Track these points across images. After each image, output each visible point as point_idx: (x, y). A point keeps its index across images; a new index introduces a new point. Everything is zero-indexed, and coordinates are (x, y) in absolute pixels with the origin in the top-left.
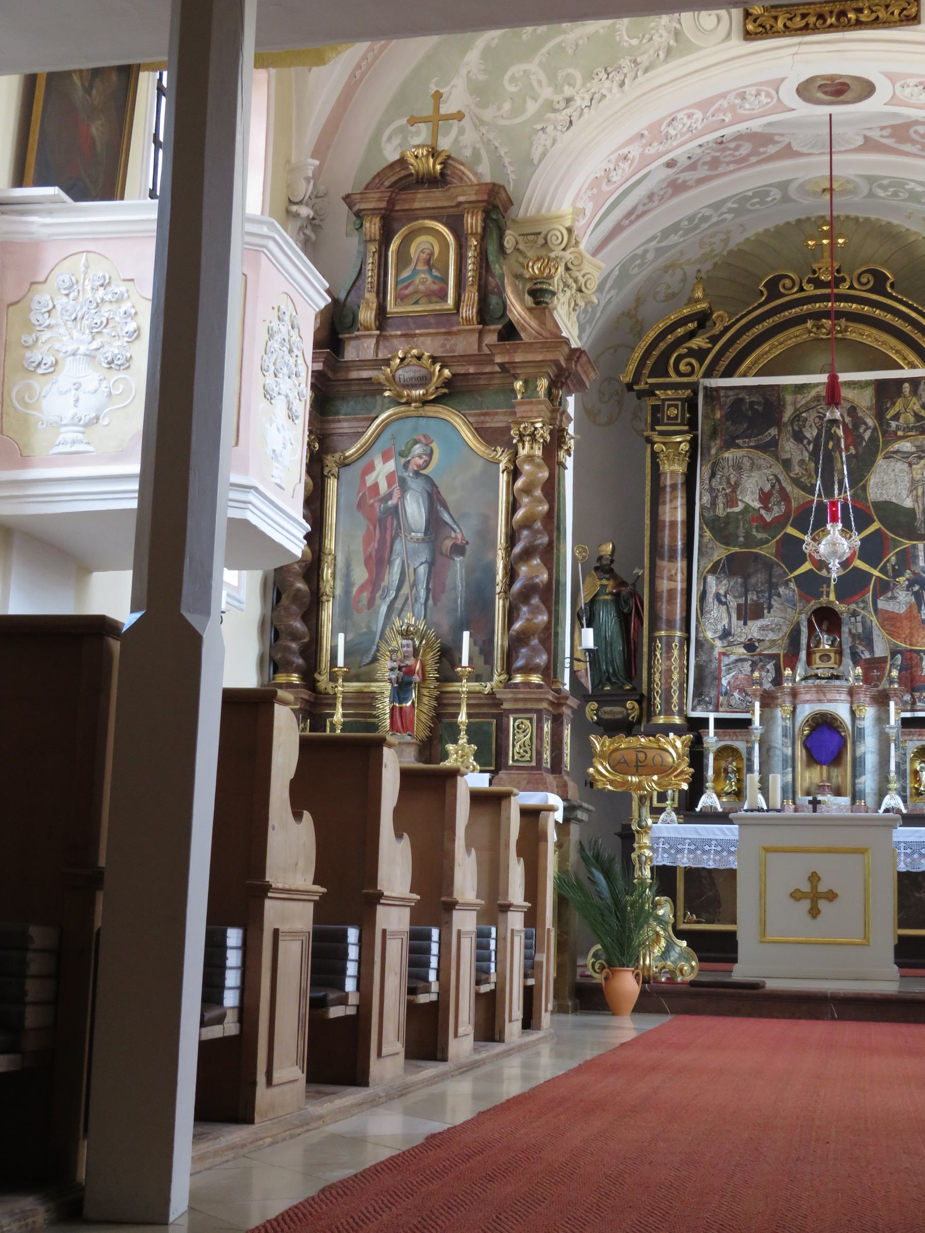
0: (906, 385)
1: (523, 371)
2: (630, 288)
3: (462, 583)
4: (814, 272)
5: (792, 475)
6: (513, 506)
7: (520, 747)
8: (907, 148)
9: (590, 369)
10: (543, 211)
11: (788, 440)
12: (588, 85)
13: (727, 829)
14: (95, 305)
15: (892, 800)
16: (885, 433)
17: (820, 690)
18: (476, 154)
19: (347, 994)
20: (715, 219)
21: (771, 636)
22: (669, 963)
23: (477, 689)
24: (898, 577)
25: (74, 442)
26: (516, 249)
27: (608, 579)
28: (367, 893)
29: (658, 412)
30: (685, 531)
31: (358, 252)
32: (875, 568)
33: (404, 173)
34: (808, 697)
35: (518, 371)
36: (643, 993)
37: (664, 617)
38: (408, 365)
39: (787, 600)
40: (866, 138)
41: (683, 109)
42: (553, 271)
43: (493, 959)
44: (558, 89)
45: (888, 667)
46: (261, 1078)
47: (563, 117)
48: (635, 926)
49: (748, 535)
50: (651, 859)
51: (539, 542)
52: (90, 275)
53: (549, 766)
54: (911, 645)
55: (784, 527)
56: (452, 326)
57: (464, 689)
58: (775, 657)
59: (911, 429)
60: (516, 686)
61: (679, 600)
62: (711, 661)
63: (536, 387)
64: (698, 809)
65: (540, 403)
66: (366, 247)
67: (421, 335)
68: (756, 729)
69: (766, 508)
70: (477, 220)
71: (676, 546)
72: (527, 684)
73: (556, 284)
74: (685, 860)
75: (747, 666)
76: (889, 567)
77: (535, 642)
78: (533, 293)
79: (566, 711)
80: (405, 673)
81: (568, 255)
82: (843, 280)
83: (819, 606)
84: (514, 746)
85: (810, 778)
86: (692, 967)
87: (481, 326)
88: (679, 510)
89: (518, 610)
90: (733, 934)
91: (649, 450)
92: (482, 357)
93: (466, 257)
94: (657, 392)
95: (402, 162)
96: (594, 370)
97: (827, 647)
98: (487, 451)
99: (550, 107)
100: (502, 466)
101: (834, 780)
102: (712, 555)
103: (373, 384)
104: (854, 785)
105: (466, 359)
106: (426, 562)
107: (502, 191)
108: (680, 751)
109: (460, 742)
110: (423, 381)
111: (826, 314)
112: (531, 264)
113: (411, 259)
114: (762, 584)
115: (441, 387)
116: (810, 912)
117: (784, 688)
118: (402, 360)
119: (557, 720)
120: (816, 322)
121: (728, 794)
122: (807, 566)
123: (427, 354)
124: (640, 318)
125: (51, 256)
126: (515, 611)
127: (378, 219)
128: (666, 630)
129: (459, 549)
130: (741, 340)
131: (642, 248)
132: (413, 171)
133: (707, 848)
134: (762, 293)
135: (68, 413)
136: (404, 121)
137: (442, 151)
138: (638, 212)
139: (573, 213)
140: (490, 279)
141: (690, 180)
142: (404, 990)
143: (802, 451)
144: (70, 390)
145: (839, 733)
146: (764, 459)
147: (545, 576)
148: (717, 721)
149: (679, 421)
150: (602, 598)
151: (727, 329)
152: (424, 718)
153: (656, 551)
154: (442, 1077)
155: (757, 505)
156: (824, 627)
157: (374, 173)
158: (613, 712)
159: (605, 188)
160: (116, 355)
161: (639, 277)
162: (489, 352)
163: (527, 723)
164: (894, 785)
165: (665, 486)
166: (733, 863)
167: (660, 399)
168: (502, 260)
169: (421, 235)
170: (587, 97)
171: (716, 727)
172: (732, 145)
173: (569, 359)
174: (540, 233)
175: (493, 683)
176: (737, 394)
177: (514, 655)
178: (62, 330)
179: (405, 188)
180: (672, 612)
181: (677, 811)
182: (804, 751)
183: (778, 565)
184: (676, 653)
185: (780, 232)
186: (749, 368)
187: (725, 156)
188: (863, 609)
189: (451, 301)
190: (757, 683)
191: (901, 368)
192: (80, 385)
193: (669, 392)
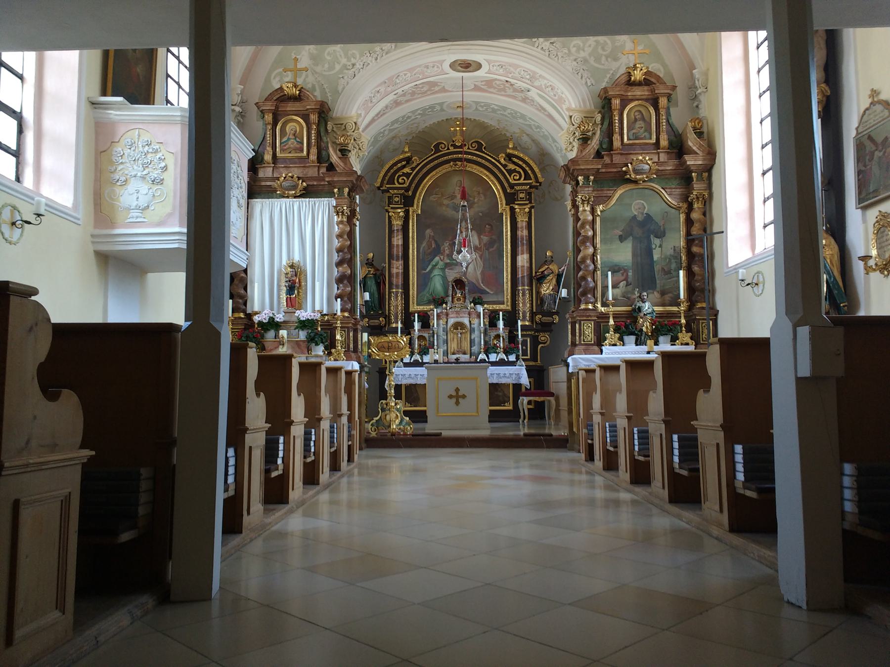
2: (378, 146)
4: (454, 141)
8: (492, 90)
12: (362, 58)
14: (144, 154)
18: (314, 86)
20: (413, 118)
22: (402, 426)
25: (137, 217)
31: (263, 128)
33: (282, 94)
34: (452, 316)
37: (394, 284)
38: (287, 180)
40: (475, 85)
41: (402, 72)
43: (335, 432)
44: (349, 60)
46: (245, 513)
47: (351, 72)
52: (141, 140)
53: (352, 350)
63: (344, 191)
65: (345, 198)
66: (266, 126)
73: (350, 147)
81: (355, 135)
82: (465, 145)
86: (411, 428)
87: (319, 164)
90: (425, 411)
91: (387, 215)
94: (390, 191)
95: (281, 89)
97: (460, 295)
99: (345, 67)
101: (463, 348)
103: (272, 188)
105: (312, 178)
107: (326, 104)
110: (294, 187)
111: (460, 160)
112: (339, 138)
113: (286, 133)
116: (451, 395)
118: (285, 178)
120: (454, 163)
123: (295, 176)
124: (383, 159)
125: (121, 130)
127: (271, 114)
131: (383, 129)
135: (134, 204)
136: (281, 70)
138: (381, 114)
140: (322, 143)
142: (302, 457)
144: (134, 193)
147: (349, 272)
150: (369, 276)
151: (418, 165)
153: (391, 257)
154: (318, 493)
157: (268, 94)
158: (375, 322)
159: (370, 105)
160: (156, 178)
161: (382, 141)
163: (343, 332)
167: (391, 194)
170: (362, 64)
172: (421, 86)
173: (357, 180)
174: (343, 124)
178: (128, 165)
179: (282, 101)
189: (305, 152)
192: (139, 191)
193: (395, 191)
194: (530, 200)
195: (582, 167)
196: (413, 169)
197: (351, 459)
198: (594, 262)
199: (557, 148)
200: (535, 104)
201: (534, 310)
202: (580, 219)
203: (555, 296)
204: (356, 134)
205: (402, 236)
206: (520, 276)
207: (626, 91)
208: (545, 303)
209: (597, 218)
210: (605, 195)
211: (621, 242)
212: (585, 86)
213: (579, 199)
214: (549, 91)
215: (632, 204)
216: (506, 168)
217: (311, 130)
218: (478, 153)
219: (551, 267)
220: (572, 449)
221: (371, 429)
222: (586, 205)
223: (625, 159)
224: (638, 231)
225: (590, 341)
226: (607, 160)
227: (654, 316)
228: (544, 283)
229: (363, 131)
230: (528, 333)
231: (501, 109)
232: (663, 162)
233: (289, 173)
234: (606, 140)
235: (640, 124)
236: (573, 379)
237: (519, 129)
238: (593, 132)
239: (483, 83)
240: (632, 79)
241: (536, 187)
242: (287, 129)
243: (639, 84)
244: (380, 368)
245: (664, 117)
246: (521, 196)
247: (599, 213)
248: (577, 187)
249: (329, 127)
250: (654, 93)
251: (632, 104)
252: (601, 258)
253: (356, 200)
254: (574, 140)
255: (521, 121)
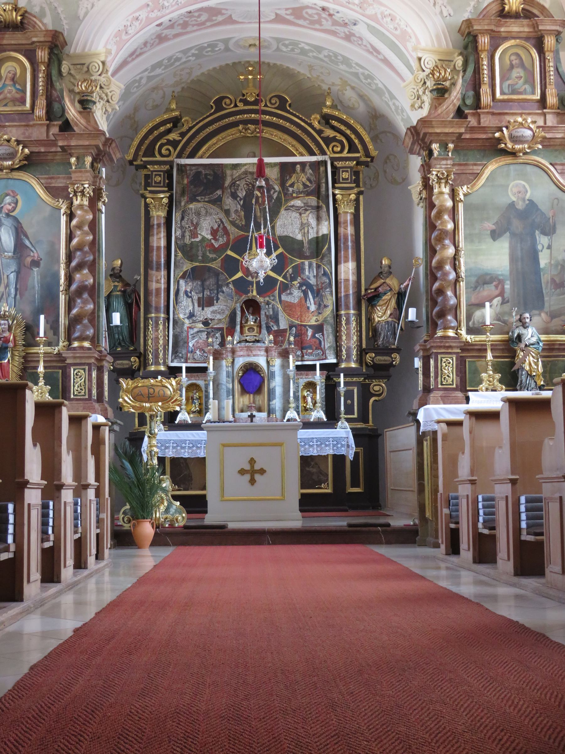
0: (298, 166)
1: (76, 151)
3: (38, 284)
4: (244, 95)
5: (230, 219)
6: (70, 237)
7: (78, 387)
8: (301, 22)
9: (117, 152)
10: (86, 50)
11: (228, 198)
13: (196, 433)
15: (291, 414)
16: (285, 194)
17: (249, 349)
18: (42, 9)
19: (9, 545)
20: (184, 60)
21: (218, 317)
23: (49, 351)
24: (293, 281)
26: (69, 74)
27: (118, 282)
28: (19, 482)
29: (149, 178)
30: (166, 252)
32: (280, 276)
34: (241, 353)
35: (73, 151)
36: (156, 534)
39: (228, 295)
40: (277, 14)
42: (94, 88)
45: (288, 335)
48: (150, 494)
49: (204, 255)
50: (157, 453)
51: (87, 259)
53: (96, 398)
54: (301, 322)
55: (226, 251)
56: (29, 121)
57: (42, 351)
58: (221, 329)
59: (301, 193)
60: (74, 349)
61: (162, 295)
62: (182, 332)
63: (85, 161)
64: (176, 422)
65: (87, 172)
67: (9, 126)
68: (211, 373)
69: (215, 239)
70: (45, 54)
71: (161, 261)
72: (82, 348)
73: (95, 97)
74: (171, 453)
75: (204, 335)
76: (288, 276)
77: (86, 321)
78: (81, 102)
79: (105, 364)
80: (3, 342)
81: (102, 79)
83: (247, 298)
84: (74, 386)
85: (243, 402)
86: (183, 517)
87: (48, 122)
88: (162, 239)
89: (75, 301)
90: (204, 496)
92: (51, 142)
93: (38, 77)
94: (148, 166)
96: (119, 152)
97: (252, 323)
98: (53, 202)
100: (62, 211)
101: (257, 403)
102: (182, 267)
104: (269, 405)
105: (39, 142)
106: (15, 271)
107: (61, 36)
108: (175, 387)
109: (40, 384)
110: (11, 156)
111: (255, 122)
112: (80, 83)
114: (213, 285)
115: (23, 160)
117: (227, 348)
119: (100, 370)
121: (194, 412)
122: (239, 275)
124: (136, 119)
126: (72, 302)
128: (155, 313)
129: (36, 263)
130: (199, 135)
131: (140, 76)
132: (2, 20)
133: (184, 445)
134: (212, 107)
137: (22, 7)
138: (137, 53)
139: (106, 53)
140: (54, 92)
141: (170, 34)
143: (236, 205)
145: (260, 374)
146: (213, 209)
148: (187, 368)
149: (162, 185)
150: (115, 293)
151: (190, 129)
152: (15, 369)
153: (148, 265)
154: (60, 593)
155: (209, 237)
156: (250, 311)
159: (124, 37)
161: (137, 93)
162: (54, 139)
163: (82, 371)
164: (292, 405)
165: (153, 225)
166: (201, 454)
167: (150, 170)
168: (60, 80)
169: (12, 61)
171: (186, 372)
172: (196, 14)
173: (104, 145)
174: (84, 64)
175: (59, 347)
176: (198, 169)
177: (72, 330)
180: (158, 302)
181: (164, 423)
182: (239, 386)
183: (222, 274)
184: (161, 327)
185: (224, 69)
186: (204, 153)
187: (192, 21)
188: (273, 300)
190: (211, 345)
191: (295, 155)
193: (156, 166)
194: (357, 182)
195: (438, 131)
196: (183, 135)
197: (100, 555)
198: (455, 268)
199: (397, 108)
200: (364, 44)
201: (364, 346)
202: (435, 206)
203: (395, 325)
204: (104, 79)
205: (165, 234)
206: (343, 294)
207: (499, 25)
208: (380, 334)
209: (460, 204)
210: (471, 172)
211: (494, 240)
212: (439, 16)
213: (433, 177)
214: (387, 22)
215: (508, 186)
216: (322, 135)
217: (38, 72)
218: (279, 112)
219: (388, 281)
220: (423, 544)
221: (123, 518)
222: (443, 185)
223: (497, 121)
224: (517, 225)
225: (450, 384)
226: (472, 121)
227: (541, 348)
228: (379, 306)
229: (113, 75)
230: (355, 379)
231: (313, 49)
232: (552, 127)
233: (5, 135)
234: (471, 93)
235: (517, 72)
236: (427, 440)
237: (341, 79)
238: (452, 81)
239: (288, 12)
240: (506, 9)
241: (366, 164)
242: (2, 71)
243: (516, 16)
244: (131, 434)
245: (551, 64)
246: (343, 176)
247: (462, 197)
248: (430, 159)
249: (65, 68)
250: (536, 29)
251: (506, 43)
252: (465, 263)
253: (102, 174)
254: (424, 93)
255: (343, 67)
